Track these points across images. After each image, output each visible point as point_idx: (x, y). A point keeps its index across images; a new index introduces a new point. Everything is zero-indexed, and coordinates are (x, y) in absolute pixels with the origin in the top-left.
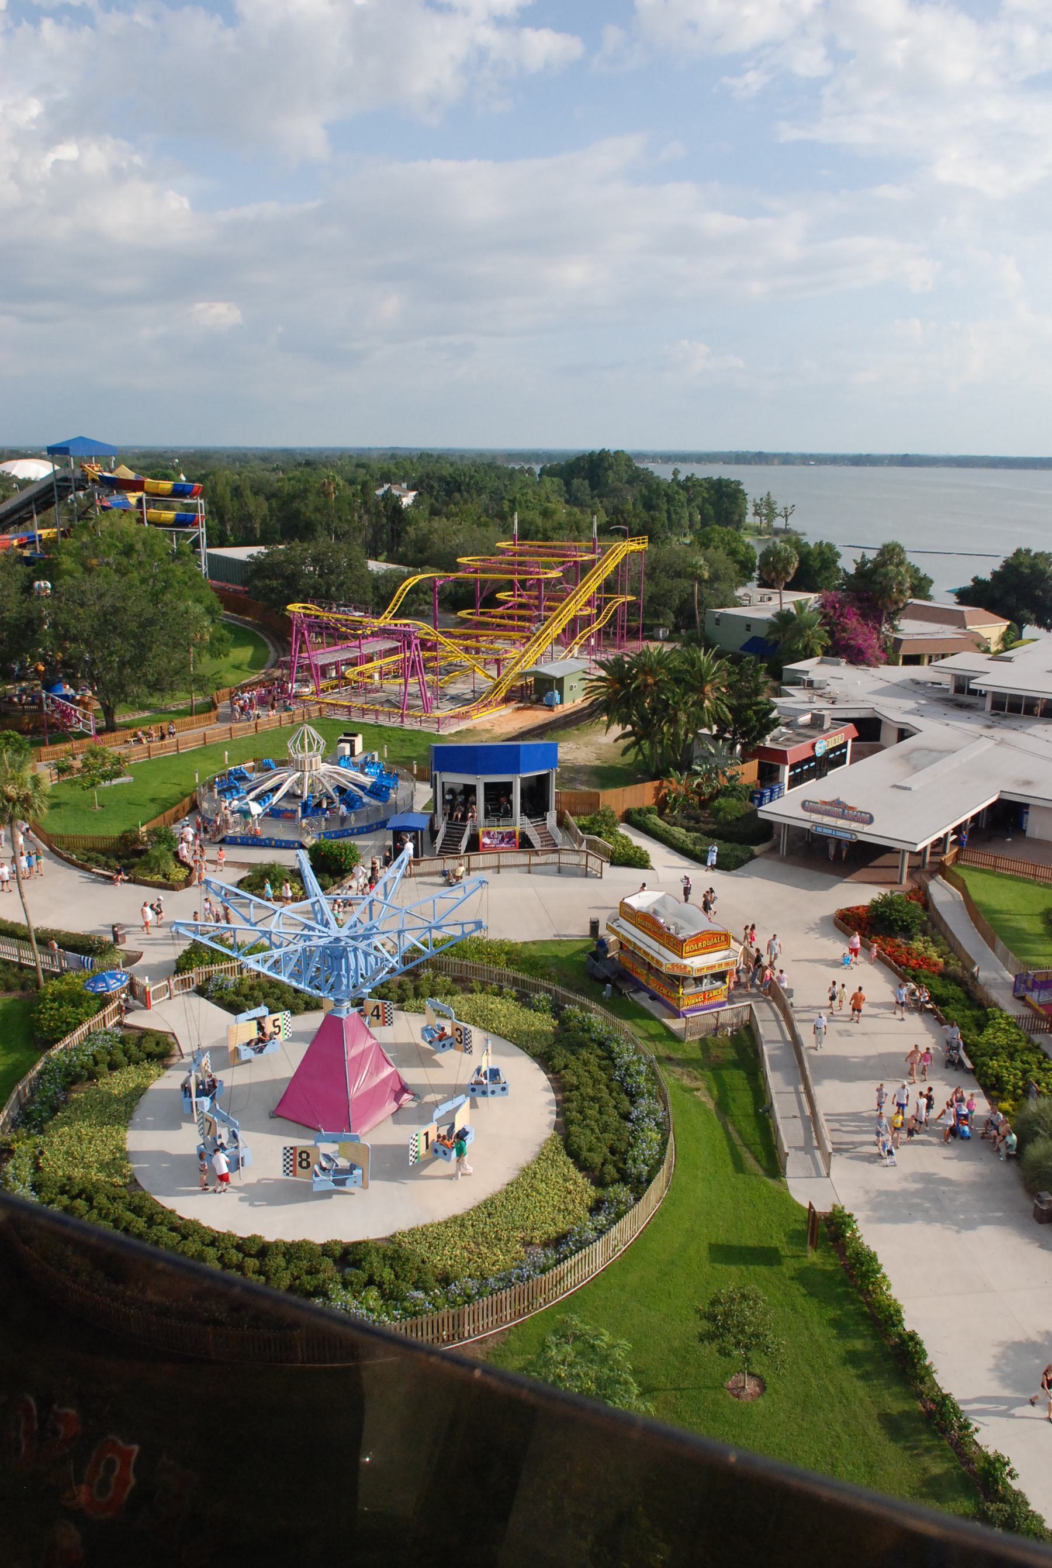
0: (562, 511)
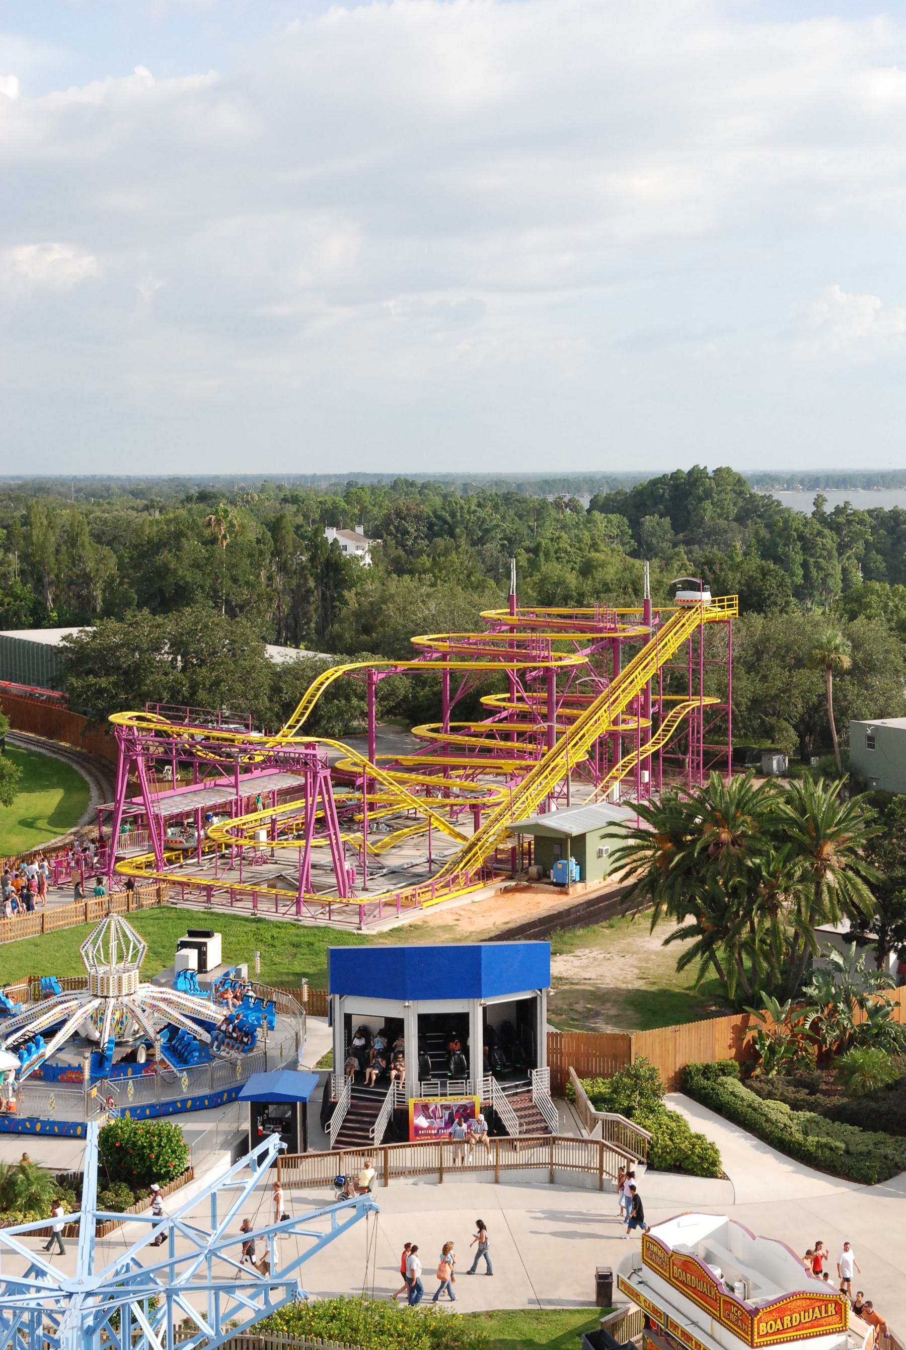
0: (613, 561)
